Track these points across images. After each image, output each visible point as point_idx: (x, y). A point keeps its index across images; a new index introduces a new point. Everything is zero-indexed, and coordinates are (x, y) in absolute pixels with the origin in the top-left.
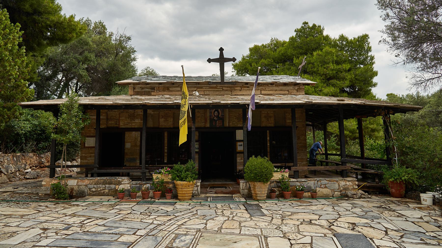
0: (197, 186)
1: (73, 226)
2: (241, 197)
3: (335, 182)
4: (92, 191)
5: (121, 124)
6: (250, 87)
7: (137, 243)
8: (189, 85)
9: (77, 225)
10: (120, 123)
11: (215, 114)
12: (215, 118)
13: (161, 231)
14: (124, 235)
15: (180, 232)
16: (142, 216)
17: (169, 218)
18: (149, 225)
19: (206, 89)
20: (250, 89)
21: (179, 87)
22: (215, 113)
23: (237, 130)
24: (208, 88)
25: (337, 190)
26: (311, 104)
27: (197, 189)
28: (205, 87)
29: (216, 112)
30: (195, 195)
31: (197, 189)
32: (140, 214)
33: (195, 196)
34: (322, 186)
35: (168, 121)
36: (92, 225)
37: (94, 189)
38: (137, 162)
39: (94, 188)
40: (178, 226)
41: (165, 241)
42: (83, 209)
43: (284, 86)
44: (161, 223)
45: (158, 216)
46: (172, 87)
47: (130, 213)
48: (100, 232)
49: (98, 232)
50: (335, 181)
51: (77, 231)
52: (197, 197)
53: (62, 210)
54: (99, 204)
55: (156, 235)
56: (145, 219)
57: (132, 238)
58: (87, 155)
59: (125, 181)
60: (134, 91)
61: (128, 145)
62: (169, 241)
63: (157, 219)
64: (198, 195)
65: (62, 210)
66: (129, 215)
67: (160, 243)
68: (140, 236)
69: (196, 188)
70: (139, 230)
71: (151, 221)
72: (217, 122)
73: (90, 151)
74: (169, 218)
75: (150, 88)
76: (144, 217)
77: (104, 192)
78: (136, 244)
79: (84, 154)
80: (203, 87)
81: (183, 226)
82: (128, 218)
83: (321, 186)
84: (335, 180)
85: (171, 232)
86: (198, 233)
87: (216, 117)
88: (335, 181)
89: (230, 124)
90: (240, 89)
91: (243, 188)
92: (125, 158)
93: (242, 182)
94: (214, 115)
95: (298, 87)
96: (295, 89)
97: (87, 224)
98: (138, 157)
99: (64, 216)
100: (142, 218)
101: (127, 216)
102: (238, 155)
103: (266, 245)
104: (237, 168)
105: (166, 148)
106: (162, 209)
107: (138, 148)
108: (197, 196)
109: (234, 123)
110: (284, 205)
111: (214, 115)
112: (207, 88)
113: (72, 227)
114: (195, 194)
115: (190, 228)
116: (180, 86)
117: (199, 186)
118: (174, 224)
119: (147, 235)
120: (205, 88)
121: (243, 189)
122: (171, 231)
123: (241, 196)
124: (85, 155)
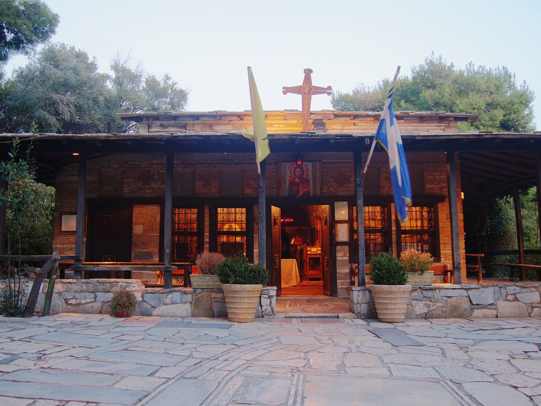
0: (271, 296)
1: (20, 358)
2: (354, 318)
3: (533, 289)
4: (71, 304)
5: (126, 191)
6: (359, 124)
7: (159, 393)
8: (248, 120)
9: (30, 356)
10: (124, 189)
11: (297, 173)
12: (297, 180)
13: (212, 370)
14: (130, 377)
15: (253, 373)
16: (168, 344)
17: (225, 348)
18: (184, 360)
19: (279, 127)
20: (359, 128)
21: (231, 124)
22: (297, 171)
23: (335, 203)
24: (283, 126)
25: (537, 305)
26: (489, 136)
27: (271, 302)
28: (277, 124)
29: (298, 170)
30: (266, 315)
31: (271, 302)
32: (164, 341)
33: (267, 316)
34: (510, 297)
35: (210, 185)
36: (61, 358)
37: (74, 300)
38: (155, 259)
39: (74, 298)
40: (246, 361)
41: (225, 389)
42: (49, 332)
43: (420, 123)
44: (209, 357)
45: (201, 345)
46: (217, 124)
47: (143, 339)
48: (77, 370)
49: (73, 370)
50: (534, 287)
51: (26, 367)
52: (271, 317)
53: (7, 331)
54: (83, 324)
55: (202, 377)
56: (174, 348)
57: (149, 383)
58: (64, 246)
59: (133, 287)
60: (148, 131)
61: (138, 229)
62: (235, 390)
63: (198, 349)
64: (272, 314)
65: (7, 331)
66: (140, 342)
67: (215, 393)
68: (165, 380)
69: (269, 300)
70: (163, 369)
71: (187, 353)
72: (301, 186)
73: (71, 240)
74: (225, 348)
75: (177, 126)
76: (171, 345)
77: (92, 307)
78: (156, 395)
79: (60, 244)
80: (274, 124)
81: (257, 363)
82: (137, 346)
83: (506, 296)
84: (534, 285)
85: (234, 373)
86: (296, 375)
87: (298, 178)
88: (534, 287)
89: (324, 191)
90: (341, 128)
91: (358, 300)
92: (132, 253)
93: (357, 289)
94: (295, 175)
95: (446, 124)
96: (441, 128)
97: (51, 356)
98: (156, 250)
99: (8, 340)
100: (168, 347)
101: (137, 344)
102: (338, 248)
103: (470, 399)
104: (337, 271)
105: (208, 234)
106: (206, 334)
107: (156, 235)
108: (271, 315)
109: (331, 189)
110: (447, 329)
111: (295, 175)
112: (281, 126)
113: (18, 358)
114: (266, 312)
115: (274, 367)
116: (231, 122)
117: (273, 296)
118: (237, 359)
119: (182, 377)
120: (278, 125)
121: (358, 303)
122: (233, 371)
123: (355, 317)
124: (61, 246)
